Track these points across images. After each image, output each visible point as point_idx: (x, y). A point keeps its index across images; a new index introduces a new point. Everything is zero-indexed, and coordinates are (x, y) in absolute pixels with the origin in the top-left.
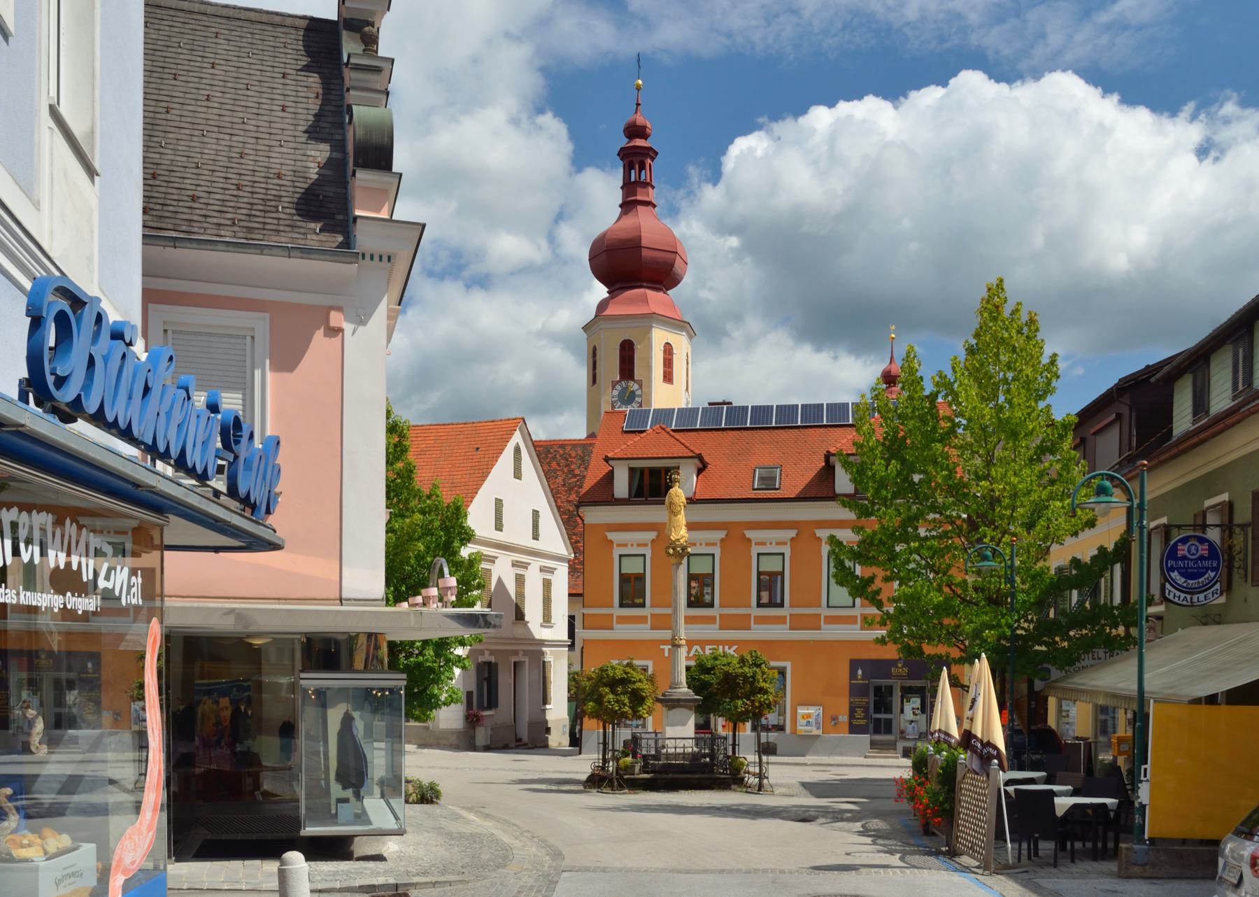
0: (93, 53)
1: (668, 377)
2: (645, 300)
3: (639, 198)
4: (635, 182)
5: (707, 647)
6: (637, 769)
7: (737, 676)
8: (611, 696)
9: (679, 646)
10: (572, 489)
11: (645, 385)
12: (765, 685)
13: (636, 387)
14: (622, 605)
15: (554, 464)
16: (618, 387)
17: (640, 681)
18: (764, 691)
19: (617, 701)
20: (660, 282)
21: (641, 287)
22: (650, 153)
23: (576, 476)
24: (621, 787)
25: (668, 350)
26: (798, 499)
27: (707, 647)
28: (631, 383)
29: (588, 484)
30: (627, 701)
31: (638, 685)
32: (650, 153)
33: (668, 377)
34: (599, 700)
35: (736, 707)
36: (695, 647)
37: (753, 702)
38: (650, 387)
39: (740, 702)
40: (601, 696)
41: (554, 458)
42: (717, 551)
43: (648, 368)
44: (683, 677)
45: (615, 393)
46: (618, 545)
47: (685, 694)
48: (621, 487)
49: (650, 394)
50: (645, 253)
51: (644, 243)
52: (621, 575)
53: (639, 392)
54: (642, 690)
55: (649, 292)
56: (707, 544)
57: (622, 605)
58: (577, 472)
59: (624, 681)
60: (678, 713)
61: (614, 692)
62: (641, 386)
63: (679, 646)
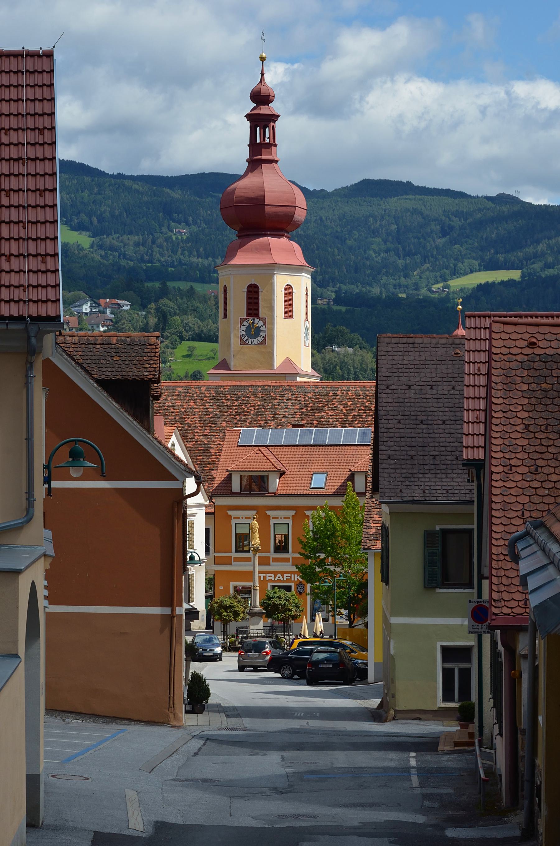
0: (29, 440)
1: (289, 314)
2: (267, 249)
3: (263, 157)
4: (260, 143)
5: (285, 575)
6: (237, 643)
7: (278, 605)
8: (225, 613)
9: (256, 590)
10: (206, 425)
11: (269, 322)
12: (291, 608)
13: (261, 323)
14: (237, 551)
15: (192, 403)
16: (245, 323)
17: (237, 606)
18: (290, 610)
19: (228, 615)
20: (282, 230)
21: (265, 235)
22: (274, 118)
23: (210, 413)
24: (230, 651)
25: (289, 291)
26: (334, 495)
27: (285, 575)
28: (256, 320)
29: (216, 483)
30: (232, 615)
31: (237, 609)
32: (274, 118)
33: (289, 314)
34: (220, 614)
35: (278, 617)
36: (278, 575)
37: (285, 615)
38: (273, 324)
39: (279, 615)
40: (221, 613)
41: (192, 397)
42: (290, 522)
43: (271, 308)
44: (258, 603)
45: (243, 328)
46: (234, 518)
47: (258, 610)
48: (236, 486)
49: (272, 330)
50: (268, 209)
51: (267, 201)
52: (236, 535)
53: (263, 328)
54: (238, 610)
55: (271, 239)
56: (285, 518)
57: (237, 551)
58: (210, 410)
59: (231, 607)
60: (255, 618)
61: (226, 611)
62: (265, 323)
63: (256, 590)
